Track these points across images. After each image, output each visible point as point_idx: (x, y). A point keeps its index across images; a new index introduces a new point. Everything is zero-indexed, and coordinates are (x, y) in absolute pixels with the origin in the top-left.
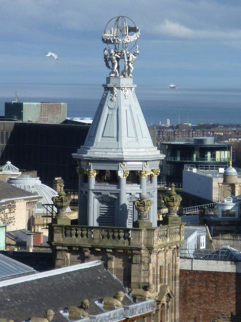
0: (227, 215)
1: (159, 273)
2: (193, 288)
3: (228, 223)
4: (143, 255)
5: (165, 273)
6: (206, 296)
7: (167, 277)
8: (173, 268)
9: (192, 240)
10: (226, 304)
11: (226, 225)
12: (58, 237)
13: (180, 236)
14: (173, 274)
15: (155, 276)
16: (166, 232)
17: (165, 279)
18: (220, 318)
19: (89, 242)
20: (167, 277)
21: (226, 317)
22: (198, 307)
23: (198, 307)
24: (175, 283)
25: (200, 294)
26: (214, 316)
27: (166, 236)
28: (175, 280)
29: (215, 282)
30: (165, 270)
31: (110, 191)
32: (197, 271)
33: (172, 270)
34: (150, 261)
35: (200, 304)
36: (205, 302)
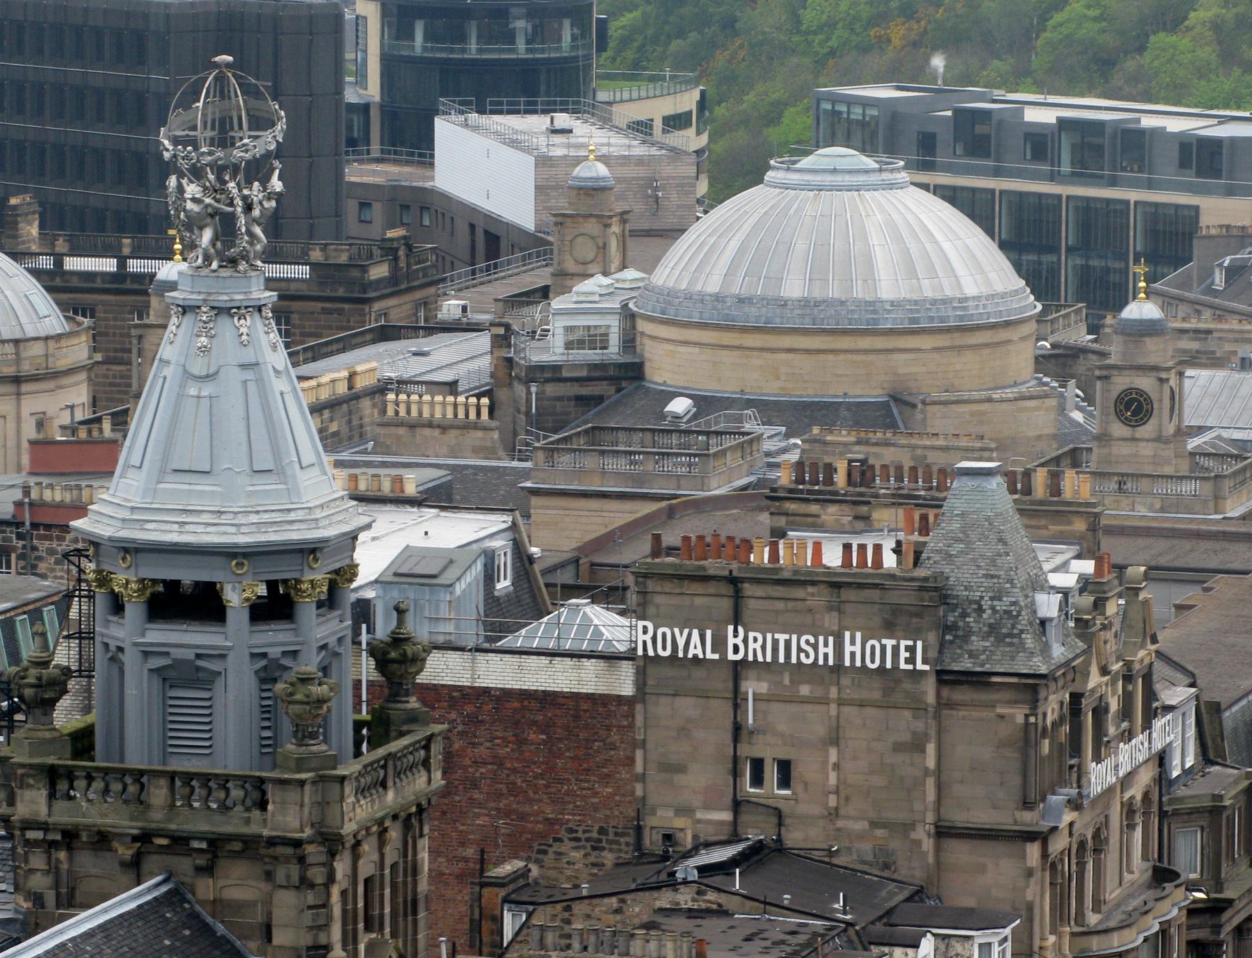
0: (580, 344)
1: (361, 904)
2: (474, 745)
3: (584, 373)
4: (310, 860)
5: (382, 896)
6: (514, 770)
7: (387, 910)
8: (405, 875)
9: (476, 579)
10: (583, 797)
11: (577, 380)
12: (32, 802)
13: (429, 771)
14: (405, 894)
15: (350, 916)
16: (382, 772)
17: (382, 916)
18: (559, 840)
19: (132, 819)
20: (387, 910)
21: (580, 835)
22: (492, 805)
23: (492, 805)
24: (415, 922)
25: (499, 762)
26: (542, 836)
27: (384, 785)
28: (415, 913)
29: (545, 727)
30: (382, 888)
31: (198, 647)
32: (486, 691)
33: (405, 883)
34: (331, 878)
35: (498, 796)
36: (513, 790)
